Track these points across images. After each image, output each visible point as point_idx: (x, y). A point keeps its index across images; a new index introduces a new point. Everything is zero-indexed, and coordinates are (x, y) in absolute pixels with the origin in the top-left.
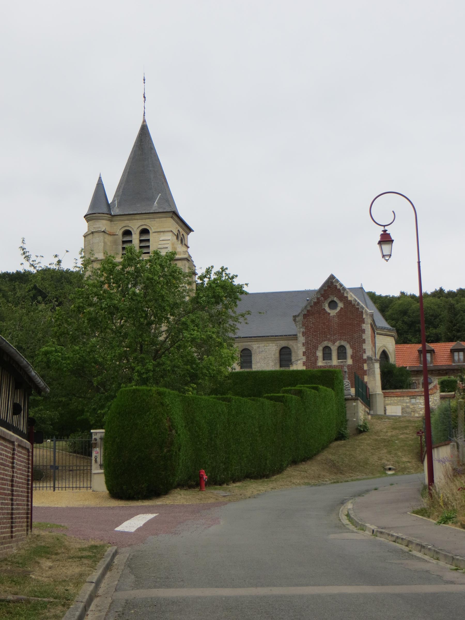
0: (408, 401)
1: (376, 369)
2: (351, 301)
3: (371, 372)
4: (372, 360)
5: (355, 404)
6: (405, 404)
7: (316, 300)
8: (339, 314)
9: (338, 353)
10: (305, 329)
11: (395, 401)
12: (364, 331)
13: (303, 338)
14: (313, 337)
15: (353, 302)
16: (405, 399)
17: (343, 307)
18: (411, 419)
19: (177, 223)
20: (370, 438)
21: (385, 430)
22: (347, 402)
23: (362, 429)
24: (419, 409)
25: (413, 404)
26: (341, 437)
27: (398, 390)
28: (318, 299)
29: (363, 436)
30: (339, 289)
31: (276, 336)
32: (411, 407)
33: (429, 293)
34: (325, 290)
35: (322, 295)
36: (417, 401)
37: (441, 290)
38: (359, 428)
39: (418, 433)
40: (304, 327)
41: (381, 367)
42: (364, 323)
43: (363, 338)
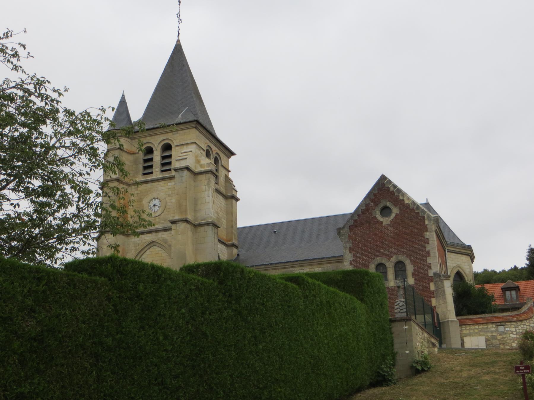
0: (493, 329)
1: (446, 289)
2: (408, 204)
3: (440, 293)
4: (440, 276)
5: (406, 327)
6: (489, 335)
7: (364, 208)
8: (394, 223)
9: (395, 271)
10: (353, 243)
11: (476, 331)
12: (428, 241)
13: (350, 255)
14: (362, 253)
15: (411, 206)
16: (489, 327)
17: (398, 213)
18: (501, 351)
19: (208, 138)
20: (431, 382)
21: (458, 369)
22: (393, 324)
23: (420, 368)
24: (511, 340)
25: (501, 333)
26: (381, 380)
27: (478, 316)
28: (367, 205)
29: (421, 379)
30: (393, 191)
31: (322, 258)
32: (499, 337)
33: (507, 270)
34: (375, 195)
35: (372, 201)
36: (507, 329)
37: (516, 268)
38: (414, 365)
39: (517, 368)
40: (351, 241)
41: (455, 288)
42: (427, 231)
43: (427, 249)
